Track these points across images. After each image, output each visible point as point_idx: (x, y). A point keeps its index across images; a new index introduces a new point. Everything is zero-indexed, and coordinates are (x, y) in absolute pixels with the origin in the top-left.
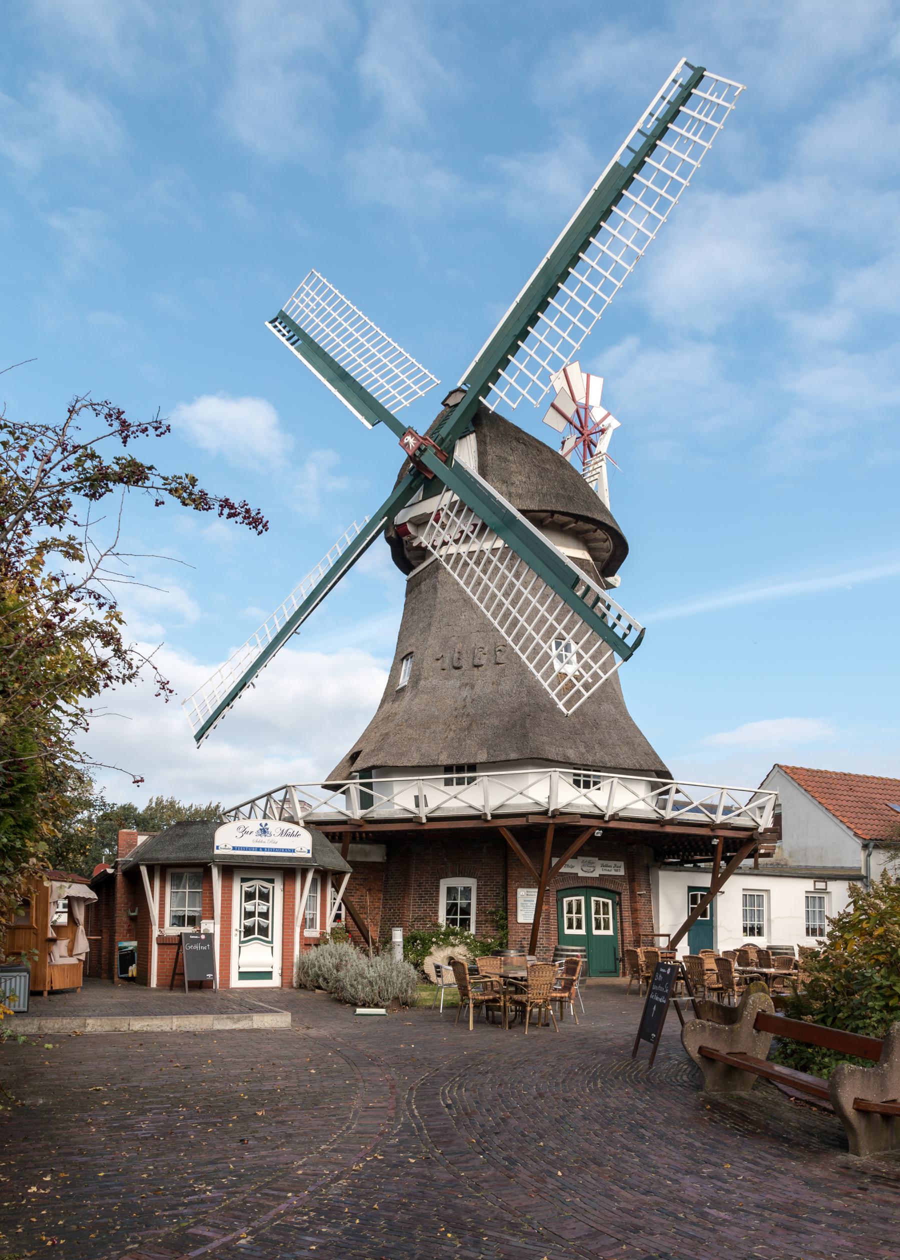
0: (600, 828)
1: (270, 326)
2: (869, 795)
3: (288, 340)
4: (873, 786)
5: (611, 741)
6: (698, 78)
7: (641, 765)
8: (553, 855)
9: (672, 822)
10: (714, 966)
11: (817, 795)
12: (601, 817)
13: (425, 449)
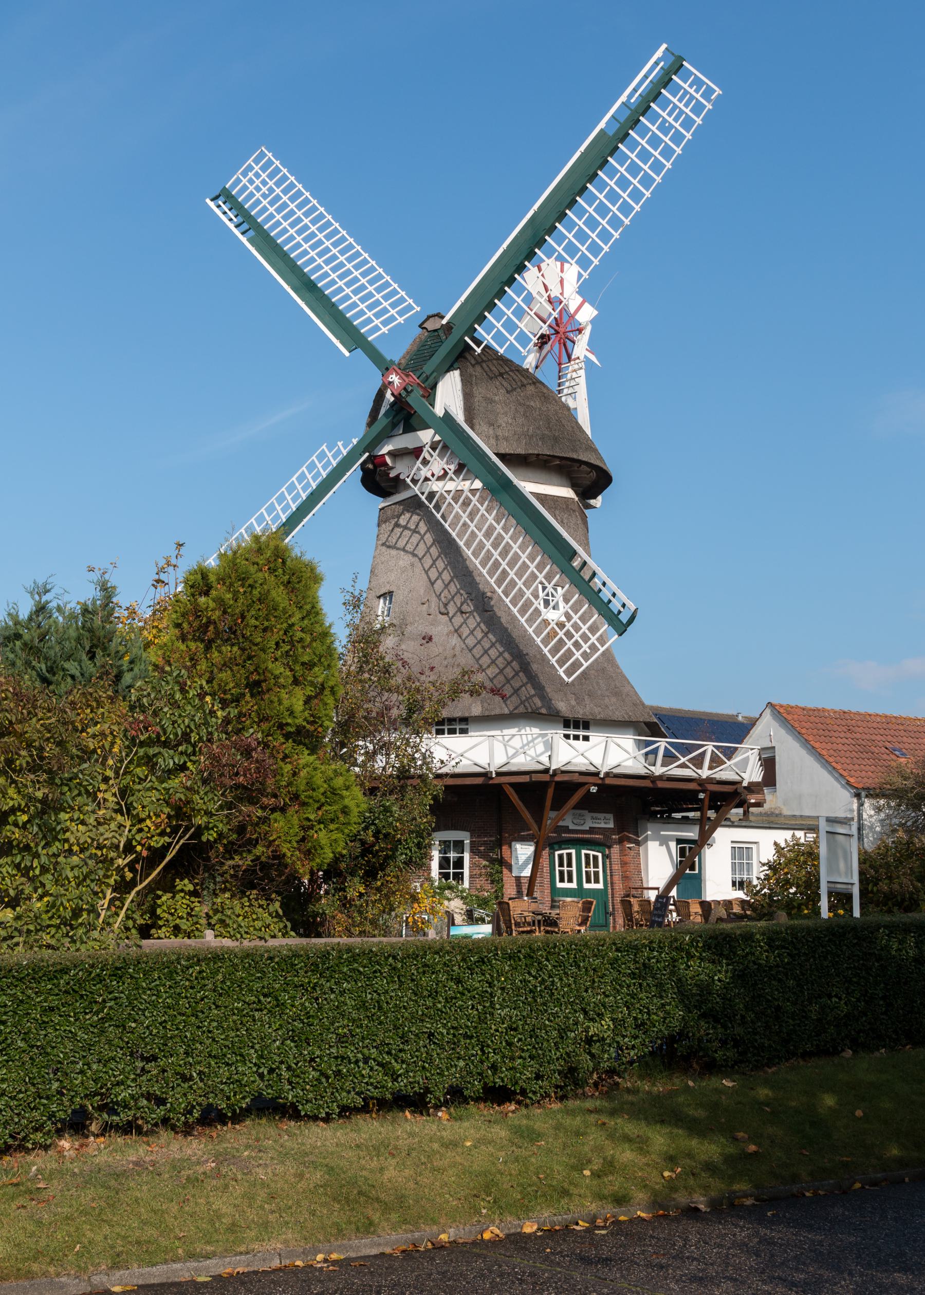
0: (595, 785)
1: (212, 205)
2: (867, 737)
3: (237, 226)
4: (875, 725)
5: (599, 692)
6: (676, 67)
7: (630, 717)
8: (552, 809)
9: (661, 777)
10: (699, 910)
11: (810, 738)
12: (596, 774)
13: (412, 391)
